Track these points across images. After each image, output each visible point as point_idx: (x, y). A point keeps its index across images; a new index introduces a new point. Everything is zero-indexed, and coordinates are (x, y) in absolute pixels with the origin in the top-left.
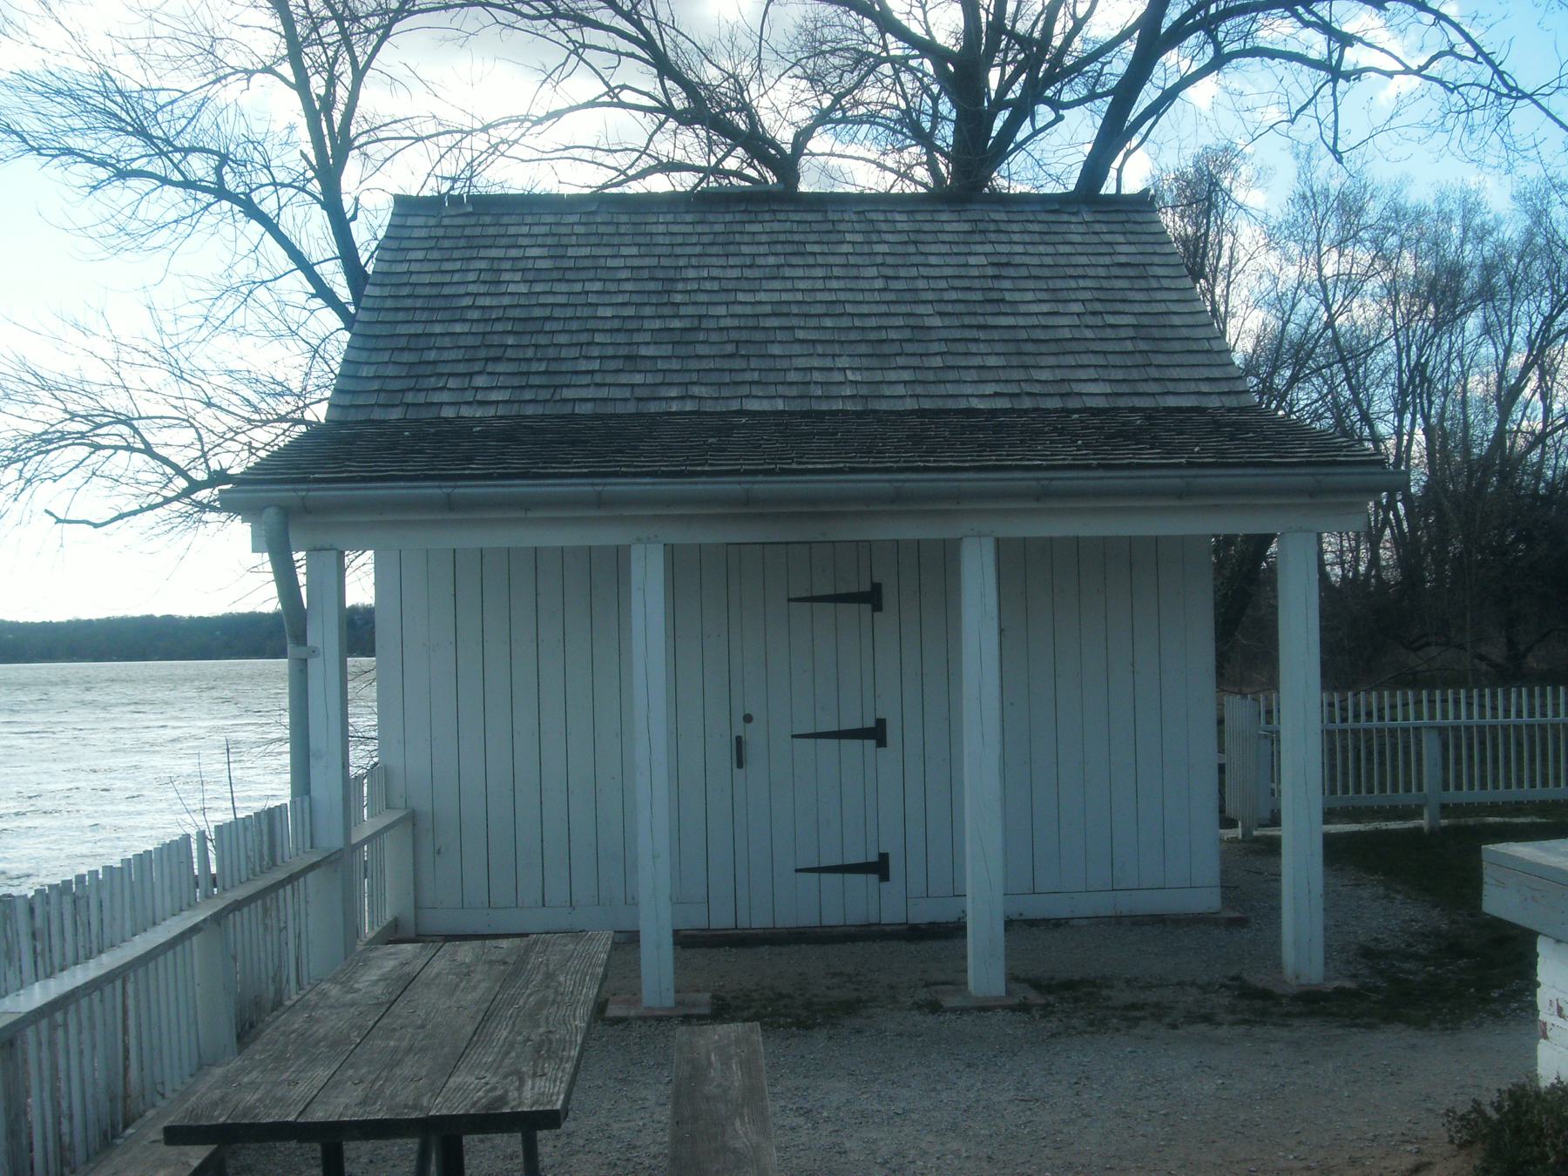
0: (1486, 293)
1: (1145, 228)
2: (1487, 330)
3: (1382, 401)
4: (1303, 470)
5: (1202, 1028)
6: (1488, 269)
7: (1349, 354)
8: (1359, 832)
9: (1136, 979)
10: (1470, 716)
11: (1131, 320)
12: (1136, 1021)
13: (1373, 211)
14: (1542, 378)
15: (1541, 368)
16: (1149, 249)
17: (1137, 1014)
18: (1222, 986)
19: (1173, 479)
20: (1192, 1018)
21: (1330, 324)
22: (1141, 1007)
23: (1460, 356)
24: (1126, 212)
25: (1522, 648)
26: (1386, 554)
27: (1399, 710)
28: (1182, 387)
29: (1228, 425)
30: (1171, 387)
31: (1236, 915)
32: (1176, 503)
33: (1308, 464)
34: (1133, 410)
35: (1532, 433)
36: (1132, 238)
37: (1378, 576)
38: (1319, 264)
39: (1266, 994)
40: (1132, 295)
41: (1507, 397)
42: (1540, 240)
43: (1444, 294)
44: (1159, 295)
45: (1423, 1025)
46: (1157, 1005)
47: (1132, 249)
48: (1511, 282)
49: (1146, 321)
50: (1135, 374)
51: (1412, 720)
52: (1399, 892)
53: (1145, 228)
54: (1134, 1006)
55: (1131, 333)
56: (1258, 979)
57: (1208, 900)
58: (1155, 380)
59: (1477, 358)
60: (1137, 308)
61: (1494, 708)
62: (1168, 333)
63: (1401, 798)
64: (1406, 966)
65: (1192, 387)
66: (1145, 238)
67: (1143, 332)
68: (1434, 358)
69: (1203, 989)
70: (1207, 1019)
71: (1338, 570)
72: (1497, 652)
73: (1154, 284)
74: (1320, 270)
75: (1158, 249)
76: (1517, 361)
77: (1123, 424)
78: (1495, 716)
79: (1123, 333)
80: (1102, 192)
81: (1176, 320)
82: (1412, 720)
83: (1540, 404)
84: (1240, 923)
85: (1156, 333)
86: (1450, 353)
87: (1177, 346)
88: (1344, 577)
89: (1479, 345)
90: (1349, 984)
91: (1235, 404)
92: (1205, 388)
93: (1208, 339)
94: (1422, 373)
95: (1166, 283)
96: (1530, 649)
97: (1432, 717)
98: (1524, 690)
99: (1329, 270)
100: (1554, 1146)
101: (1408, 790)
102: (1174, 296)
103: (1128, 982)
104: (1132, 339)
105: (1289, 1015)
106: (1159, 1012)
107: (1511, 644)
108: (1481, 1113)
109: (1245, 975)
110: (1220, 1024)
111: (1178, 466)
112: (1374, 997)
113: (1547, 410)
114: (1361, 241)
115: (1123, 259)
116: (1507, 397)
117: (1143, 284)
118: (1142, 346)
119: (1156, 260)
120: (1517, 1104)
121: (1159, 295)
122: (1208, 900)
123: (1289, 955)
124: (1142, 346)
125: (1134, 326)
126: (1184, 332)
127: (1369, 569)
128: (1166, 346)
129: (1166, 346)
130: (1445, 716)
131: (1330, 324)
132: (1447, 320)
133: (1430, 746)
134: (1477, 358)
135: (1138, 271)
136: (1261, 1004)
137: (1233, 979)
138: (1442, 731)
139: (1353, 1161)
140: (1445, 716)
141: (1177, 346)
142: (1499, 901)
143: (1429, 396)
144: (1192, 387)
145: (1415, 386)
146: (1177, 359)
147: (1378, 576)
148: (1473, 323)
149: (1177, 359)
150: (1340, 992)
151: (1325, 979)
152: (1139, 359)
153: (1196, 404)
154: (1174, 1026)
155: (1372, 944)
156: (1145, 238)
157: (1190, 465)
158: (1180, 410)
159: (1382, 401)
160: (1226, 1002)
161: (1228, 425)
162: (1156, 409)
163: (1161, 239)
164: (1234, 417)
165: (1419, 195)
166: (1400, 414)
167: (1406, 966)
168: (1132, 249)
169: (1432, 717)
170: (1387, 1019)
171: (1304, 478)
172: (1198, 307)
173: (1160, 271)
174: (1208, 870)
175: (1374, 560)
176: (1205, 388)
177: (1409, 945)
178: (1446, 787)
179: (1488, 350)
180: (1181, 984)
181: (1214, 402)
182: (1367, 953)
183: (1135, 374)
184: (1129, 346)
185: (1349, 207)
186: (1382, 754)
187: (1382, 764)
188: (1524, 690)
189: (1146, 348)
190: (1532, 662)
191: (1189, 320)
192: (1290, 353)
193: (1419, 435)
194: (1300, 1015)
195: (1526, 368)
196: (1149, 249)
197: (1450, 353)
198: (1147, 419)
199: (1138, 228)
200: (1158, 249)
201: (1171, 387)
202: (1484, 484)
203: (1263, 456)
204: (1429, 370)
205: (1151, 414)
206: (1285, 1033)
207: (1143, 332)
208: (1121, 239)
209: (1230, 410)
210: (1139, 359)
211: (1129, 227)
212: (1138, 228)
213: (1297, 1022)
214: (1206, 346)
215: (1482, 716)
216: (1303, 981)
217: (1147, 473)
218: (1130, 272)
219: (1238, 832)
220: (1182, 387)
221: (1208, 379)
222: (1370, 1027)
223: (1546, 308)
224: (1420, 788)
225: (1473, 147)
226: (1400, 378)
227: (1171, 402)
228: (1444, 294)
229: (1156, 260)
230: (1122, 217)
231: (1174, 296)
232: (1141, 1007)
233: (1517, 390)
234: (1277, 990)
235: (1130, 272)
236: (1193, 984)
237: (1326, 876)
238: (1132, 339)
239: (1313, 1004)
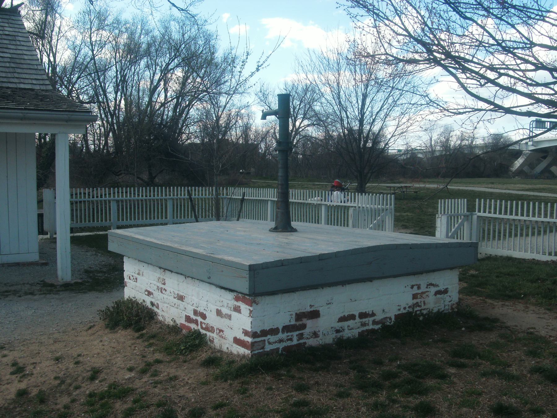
0: (148, 53)
1: (16, 22)
2: (148, 66)
3: (110, 89)
4: (63, 113)
5: (30, 296)
6: (149, 45)
7: (100, 71)
8: (90, 235)
9: (8, 283)
10: (126, 196)
11: (9, 55)
12: (7, 296)
13: (110, 20)
14: (165, 85)
15: (165, 81)
16: (17, 30)
17: (6, 294)
18: (38, 283)
19: (19, 114)
20: (26, 294)
21: (93, 58)
22: (10, 291)
23: (138, 74)
24: (9, 15)
25: (154, 175)
26: (110, 142)
27: (102, 194)
28: (26, 81)
29: (40, 96)
30: (22, 81)
31: (44, 262)
32: (20, 122)
33: (66, 111)
34: (8, 88)
35: (161, 103)
36: (11, 25)
37: (107, 149)
38: (90, 35)
39: (52, 285)
40: (10, 46)
41: (153, 91)
42: (167, 37)
43: (133, 52)
44: (20, 48)
45: (101, 291)
46: (14, 291)
47: (11, 29)
48: (157, 50)
49: (14, 56)
50: (9, 75)
51: (107, 198)
52: (99, 253)
53: (16, 22)
54: (7, 291)
55: (9, 60)
56: (48, 281)
57: (35, 257)
58: (17, 78)
59: (144, 76)
60: (12, 51)
61: (134, 194)
62: (22, 61)
63: (104, 223)
64: (99, 275)
65: (30, 81)
66: (16, 26)
67: (13, 60)
68: (129, 74)
69: (32, 285)
70: (32, 294)
71: (93, 147)
72: (145, 177)
73: (18, 43)
74: (91, 38)
75: (20, 31)
76: (157, 77)
77: (4, 93)
78: (135, 196)
79: (6, 60)
80: (3, 5)
81: (26, 57)
82: (107, 198)
83: (164, 94)
84: (46, 264)
85: (18, 61)
86: (134, 73)
87: (25, 66)
88: (95, 149)
89: (144, 71)
90: (80, 281)
91: (45, 89)
92: (34, 82)
93: (37, 65)
94: (125, 78)
95: (23, 43)
96: (156, 176)
97: (114, 197)
98: (144, 188)
99: (94, 39)
100: (126, 315)
101: (106, 220)
102: (25, 48)
103: (5, 284)
104: (9, 62)
105: (59, 291)
106: (15, 293)
107: (150, 174)
108: (109, 310)
109: (46, 280)
110: (35, 295)
111: (22, 109)
112: (87, 284)
113: (166, 96)
114: (105, 30)
115: (7, 33)
116: (153, 91)
117: (14, 43)
118: (13, 65)
119: (20, 34)
120: (118, 305)
121: (20, 48)
122: (35, 257)
123: (60, 273)
124: (13, 65)
125: (10, 58)
126: (28, 62)
127: (104, 147)
128: (21, 66)
129: (21, 66)
130: (118, 196)
131: (93, 58)
132: (134, 62)
133: (114, 206)
134: (144, 76)
135: (13, 38)
136: (50, 288)
137: (41, 281)
138: (118, 201)
139: (73, 329)
140: (118, 196)
141: (25, 66)
142: (112, 247)
143: (126, 87)
144: (30, 81)
145: (122, 84)
146: (25, 71)
147: (107, 149)
148: (143, 63)
149: (25, 71)
150: (76, 283)
151: (72, 280)
152: (11, 70)
153: (31, 87)
154: (20, 296)
155: (89, 269)
156: (16, 26)
157: (25, 109)
158: (25, 89)
159: (110, 89)
160: (38, 288)
161: (40, 96)
162: (16, 88)
163: (22, 27)
164: (44, 93)
165: (127, 16)
166: (116, 93)
167: (99, 275)
168: (11, 29)
169: (114, 197)
170: (90, 290)
171: (65, 116)
172: (34, 53)
173: (21, 39)
174: (35, 248)
175: (106, 143)
176: (34, 82)
177: (101, 269)
178: (119, 220)
179: (147, 73)
180: (24, 284)
181: (37, 87)
182: (86, 271)
183: (9, 75)
184: (8, 65)
185: (101, 17)
186: (102, 210)
187: (102, 214)
188: (144, 188)
189: (14, 66)
190: (157, 180)
191: (30, 57)
192: (78, 67)
193: (123, 102)
194: (62, 291)
195: (160, 80)
196: (17, 30)
197: (134, 73)
198: (12, 91)
199: (13, 22)
200: (20, 31)
201: (22, 81)
202: (143, 120)
203: (51, 107)
204: (127, 78)
205: (14, 90)
206: (57, 296)
207: (13, 60)
208: (7, 25)
209: (43, 90)
210: (11, 70)
211: (10, 21)
212: (13, 22)
213: (61, 293)
214: (36, 67)
215: (130, 196)
216: (64, 280)
217: (10, 111)
218: (10, 38)
219: (48, 236)
220: (26, 81)
221: (36, 79)
222: (85, 293)
223: (167, 60)
224: (110, 220)
225: (139, 4)
226: (117, 81)
227: (22, 86)
228: (133, 52)
229: (20, 34)
230: (8, 17)
231: (25, 48)
232: (10, 291)
233: (156, 87)
234: (56, 284)
235: (10, 38)
236: (28, 284)
237: (71, 246)
238: (9, 62)
239: (67, 287)
